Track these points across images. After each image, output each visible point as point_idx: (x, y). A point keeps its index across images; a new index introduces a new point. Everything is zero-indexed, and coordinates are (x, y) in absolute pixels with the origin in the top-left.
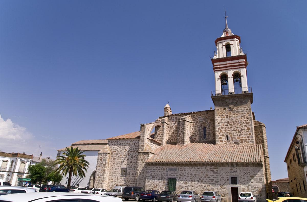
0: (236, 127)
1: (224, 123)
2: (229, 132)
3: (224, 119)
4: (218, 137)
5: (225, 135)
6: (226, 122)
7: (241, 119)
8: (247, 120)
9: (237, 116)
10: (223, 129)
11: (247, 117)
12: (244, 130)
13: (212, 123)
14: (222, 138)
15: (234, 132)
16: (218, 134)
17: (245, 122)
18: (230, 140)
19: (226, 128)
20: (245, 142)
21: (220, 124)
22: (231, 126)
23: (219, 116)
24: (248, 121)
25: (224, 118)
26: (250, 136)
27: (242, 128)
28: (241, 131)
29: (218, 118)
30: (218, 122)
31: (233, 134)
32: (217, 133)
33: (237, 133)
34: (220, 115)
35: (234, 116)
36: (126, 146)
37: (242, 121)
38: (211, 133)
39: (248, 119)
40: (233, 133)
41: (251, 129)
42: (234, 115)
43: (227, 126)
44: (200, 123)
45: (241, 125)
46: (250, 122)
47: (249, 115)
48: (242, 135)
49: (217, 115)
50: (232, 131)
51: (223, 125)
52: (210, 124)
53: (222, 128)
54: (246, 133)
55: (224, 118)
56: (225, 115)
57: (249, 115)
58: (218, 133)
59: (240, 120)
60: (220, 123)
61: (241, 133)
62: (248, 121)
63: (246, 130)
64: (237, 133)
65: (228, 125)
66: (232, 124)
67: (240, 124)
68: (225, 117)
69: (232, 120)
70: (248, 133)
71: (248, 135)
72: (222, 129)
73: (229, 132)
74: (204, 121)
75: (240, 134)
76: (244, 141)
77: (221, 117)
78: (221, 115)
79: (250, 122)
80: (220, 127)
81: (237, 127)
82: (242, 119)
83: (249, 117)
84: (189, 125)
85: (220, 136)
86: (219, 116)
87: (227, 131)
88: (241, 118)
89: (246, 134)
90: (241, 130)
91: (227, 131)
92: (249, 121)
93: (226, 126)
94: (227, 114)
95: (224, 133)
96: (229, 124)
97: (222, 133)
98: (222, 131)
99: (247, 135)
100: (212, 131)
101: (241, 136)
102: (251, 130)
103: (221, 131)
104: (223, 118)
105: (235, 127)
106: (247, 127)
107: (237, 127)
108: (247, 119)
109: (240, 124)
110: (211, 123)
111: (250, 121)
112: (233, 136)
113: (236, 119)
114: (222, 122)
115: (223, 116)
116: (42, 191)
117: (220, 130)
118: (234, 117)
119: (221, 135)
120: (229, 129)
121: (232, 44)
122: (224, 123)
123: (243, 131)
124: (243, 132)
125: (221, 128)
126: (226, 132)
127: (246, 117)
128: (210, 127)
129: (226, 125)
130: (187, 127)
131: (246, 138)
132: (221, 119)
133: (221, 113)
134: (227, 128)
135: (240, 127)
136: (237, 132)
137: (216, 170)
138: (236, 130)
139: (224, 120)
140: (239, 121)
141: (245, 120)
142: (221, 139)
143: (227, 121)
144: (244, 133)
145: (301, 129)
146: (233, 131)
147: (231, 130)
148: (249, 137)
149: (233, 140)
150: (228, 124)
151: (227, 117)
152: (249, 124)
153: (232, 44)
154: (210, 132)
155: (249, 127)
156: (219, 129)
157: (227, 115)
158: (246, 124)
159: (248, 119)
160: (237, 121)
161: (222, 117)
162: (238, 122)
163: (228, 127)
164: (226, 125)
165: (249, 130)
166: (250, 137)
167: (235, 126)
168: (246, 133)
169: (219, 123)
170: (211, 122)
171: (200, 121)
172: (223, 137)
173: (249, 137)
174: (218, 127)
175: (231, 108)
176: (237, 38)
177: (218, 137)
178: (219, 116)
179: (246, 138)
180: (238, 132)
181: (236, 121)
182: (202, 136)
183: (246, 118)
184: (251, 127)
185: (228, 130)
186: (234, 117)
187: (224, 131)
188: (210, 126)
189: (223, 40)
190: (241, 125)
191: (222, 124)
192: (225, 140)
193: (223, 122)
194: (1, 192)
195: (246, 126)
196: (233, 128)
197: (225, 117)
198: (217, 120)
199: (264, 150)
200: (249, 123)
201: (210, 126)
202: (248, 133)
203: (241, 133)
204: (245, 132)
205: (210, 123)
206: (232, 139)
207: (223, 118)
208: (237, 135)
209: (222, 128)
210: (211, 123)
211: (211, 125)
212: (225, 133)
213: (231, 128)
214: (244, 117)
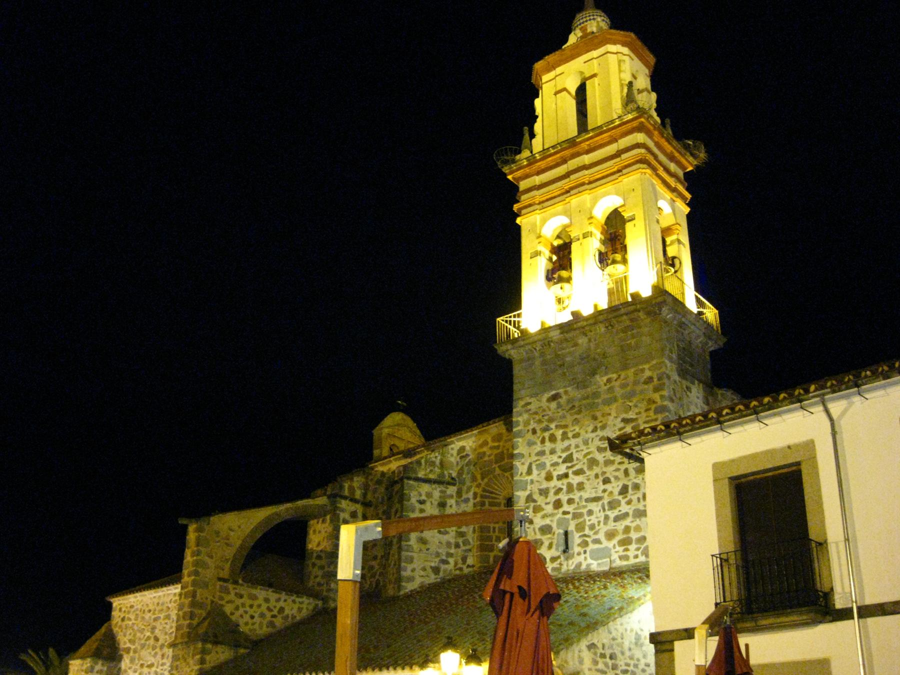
6: (560, 460)
18: (577, 549)
19: (559, 491)
20: (639, 553)
28: (620, 498)
30: (526, 467)
33: (604, 510)
34: (534, 432)
36: (228, 613)
43: (565, 481)
44: (483, 483)
53: (544, 492)
64: (604, 510)
74: (497, 469)
75: (616, 512)
76: (633, 547)
80: (535, 488)
81: (606, 481)
84: (429, 495)
90: (620, 493)
91: (566, 507)
95: (552, 515)
96: (575, 469)
97: (543, 517)
114: (542, 466)
116: (880, 613)
121: (594, 75)
126: (561, 510)
129: (560, 478)
130: (418, 506)
133: (540, 421)
138: (600, 494)
143: (564, 455)
149: (588, 549)
150: (570, 471)
153: (594, 75)
156: (530, 499)
164: (560, 478)
171: (482, 474)
176: (615, 43)
182: (491, 533)
185: (570, 501)
189: (559, 65)
192: (556, 554)
194: (549, 674)
199: (840, 562)
203: (624, 508)
206: (585, 544)
208: (607, 518)
209: (541, 494)
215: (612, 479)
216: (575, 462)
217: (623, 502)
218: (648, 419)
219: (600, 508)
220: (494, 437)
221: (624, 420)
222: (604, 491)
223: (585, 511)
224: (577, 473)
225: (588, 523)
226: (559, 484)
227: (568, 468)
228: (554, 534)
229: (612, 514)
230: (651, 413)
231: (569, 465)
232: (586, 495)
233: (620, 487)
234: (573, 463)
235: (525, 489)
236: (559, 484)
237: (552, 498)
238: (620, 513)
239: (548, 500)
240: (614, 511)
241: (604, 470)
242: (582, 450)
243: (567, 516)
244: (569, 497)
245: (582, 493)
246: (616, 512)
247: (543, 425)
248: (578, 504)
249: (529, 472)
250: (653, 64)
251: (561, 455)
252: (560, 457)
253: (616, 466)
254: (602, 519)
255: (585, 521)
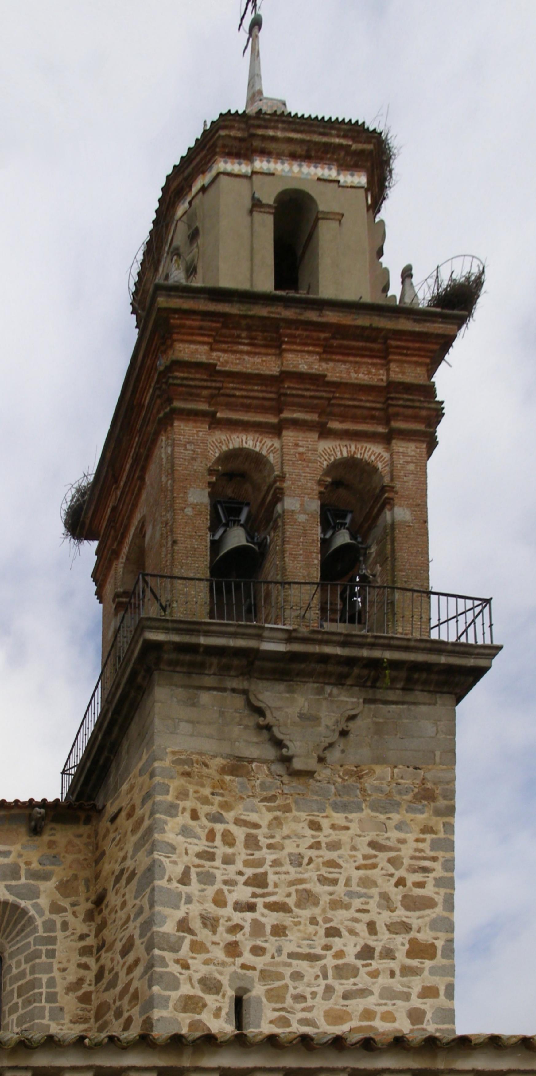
0: (322, 932)
1: (226, 882)
2: (260, 962)
3: (229, 851)
4: (174, 995)
5: (225, 980)
6: (242, 879)
7: (366, 867)
8: (418, 877)
9: (335, 836)
10: (214, 932)
11: (412, 858)
12: (389, 954)
13: (74, 913)
14: (205, 1005)
15: (302, 966)
16: (174, 969)
17: (396, 894)
19: (236, 928)
21: (194, 887)
22: (281, 914)
23: (184, 819)
24: (421, 885)
25: (229, 840)
26: (428, 1005)
27: (372, 944)
28: (359, 963)
29: (181, 838)
30: (180, 869)
31: (291, 983)
32: (168, 956)
34: (195, 815)
35: (309, 832)
37: (375, 884)
38: (60, 989)
39: (425, 870)
40: (297, 976)
41: (443, 956)
42: (315, 826)
43: (249, 916)
45: (366, 918)
46: (439, 899)
47: (435, 845)
48: (364, 993)
49: (172, 810)
50: (284, 958)
51: (219, 901)
52: (58, 919)
54: (397, 984)
55: (229, 840)
56: (239, 822)
57: (435, 845)
58: (177, 961)
59: (361, 872)
60: (194, 877)
61: (363, 980)
62: (421, 885)
63: (401, 955)
64: (325, 977)
65: (251, 908)
66: (291, 902)
67: (359, 911)
68: (240, 833)
69: (292, 870)
70: (416, 984)
71: (416, 1002)
72: (204, 935)
73: (260, 962)
75: (348, 984)
77: (203, 834)
78: (203, 810)
79: (439, 899)
80: (195, 910)
81: (333, 932)
82: (374, 866)
83: (434, 859)
85: (185, 989)
86: (184, 819)
87: (247, 958)
88: (365, 857)
89: (399, 988)
90: (359, 956)
91: (247, 958)
92: (429, 891)
93: (241, 911)
94: (253, 817)
95: (223, 964)
97: (206, 963)
98: (208, 952)
99: (407, 997)
100: (72, 978)
101: (357, 1005)
102: (445, 962)
103: (197, 947)
104: (218, 841)
105: (311, 929)
106: (413, 934)
107: (333, 932)
108: (414, 870)
109: (359, 911)
110: (65, 910)
111: (442, 891)
112: (289, 1001)
113: (332, 864)
115: (219, 827)
117: (189, 938)
118: (316, 846)
119: (197, 977)
120: (259, 943)
122: (226, 882)
123: (376, 964)
124: (374, 974)
125: (196, 924)
126: (239, 961)
127: (406, 852)
128: (52, 941)
129: (240, 907)
131: (394, 1020)
132: (201, 845)
134: (247, 929)
135: (352, 932)
136: (330, 973)
137: (390, 861)
138: (318, 951)
139: (228, 860)
140: (354, 882)
141: (401, 882)
142: (194, 1011)
143: (249, 872)
144: (384, 980)
145: (272, 131)
146: (294, 962)
147: (279, 950)
148: (424, 1013)
150: (260, 902)
151: (248, 836)
152: (431, 914)
154: (51, 983)
155: (425, 936)
156: (184, 925)
157: (256, 826)
158: (401, 914)
159: (425, 870)
160: (335, 882)
161: (211, 836)
162: (340, 889)
163: (257, 928)
164: (240, 907)
165: (428, 964)
166: (429, 1016)
167: (313, 921)
168: (397, 984)
169: (184, 880)
170: (65, 903)
172: (211, 1000)
173: (424, 1013)
174: (177, 907)
175: (297, 764)
177: (174, 995)
178: (187, 815)
179: (394, 1020)
180: (336, 967)
181: (323, 880)
183: (406, 862)
184: (440, 934)
185: (258, 951)
186: (316, 846)
187: (219, 954)
188: (59, 934)
190: (366, 918)
191: (211, 891)
193: (218, 873)
195: (407, 928)
196: (293, 935)
197: (240, 833)
198: (173, 848)
200: (429, 903)
201: (59, 934)
202: (416, 984)
203: (363, 980)
204: (392, 974)
205: (56, 908)
207: (218, 841)
208: (329, 990)
209: (205, 925)
210: (65, 910)
211: (65, 926)
212: (232, 969)
213: (279, 931)
214: (392, 854)
215: (345, 933)
216: (270, 889)
217: (363, 971)
218: (417, 854)
219: (317, 971)
220: (88, 821)
221: (373, 844)
222: (327, 947)
223: (287, 972)
224: (273, 907)
225: (291, 991)
226: (237, 917)
227: (254, 895)
228: (224, 996)
229: (341, 987)
230: (425, 846)
231: (259, 891)
232: (290, 947)
233: (359, 948)
234: (265, 891)
235: (177, 907)
236: (237, 917)
237: (223, 936)
238: (354, 988)
239: (216, 938)
240: (343, 981)
241: (330, 914)
242: (287, 873)
243: (249, 973)
244: (254, 943)
245: (282, 941)
246: (348, 984)
247: (214, 809)
248: (273, 957)
249: (184, 880)
250: (157, 721)
251: (245, 870)
252: (240, 873)
253: (351, 913)
254: (320, 990)
255: (287, 986)
